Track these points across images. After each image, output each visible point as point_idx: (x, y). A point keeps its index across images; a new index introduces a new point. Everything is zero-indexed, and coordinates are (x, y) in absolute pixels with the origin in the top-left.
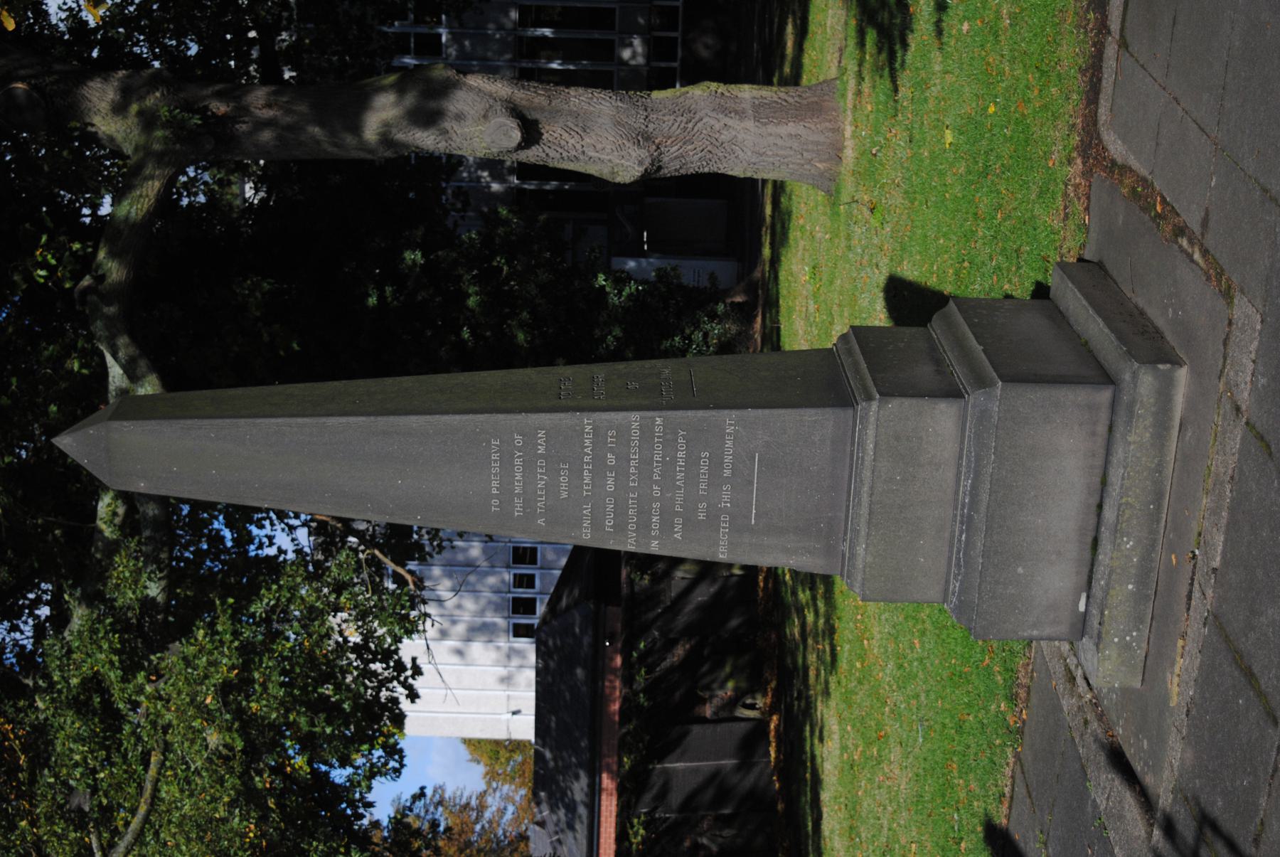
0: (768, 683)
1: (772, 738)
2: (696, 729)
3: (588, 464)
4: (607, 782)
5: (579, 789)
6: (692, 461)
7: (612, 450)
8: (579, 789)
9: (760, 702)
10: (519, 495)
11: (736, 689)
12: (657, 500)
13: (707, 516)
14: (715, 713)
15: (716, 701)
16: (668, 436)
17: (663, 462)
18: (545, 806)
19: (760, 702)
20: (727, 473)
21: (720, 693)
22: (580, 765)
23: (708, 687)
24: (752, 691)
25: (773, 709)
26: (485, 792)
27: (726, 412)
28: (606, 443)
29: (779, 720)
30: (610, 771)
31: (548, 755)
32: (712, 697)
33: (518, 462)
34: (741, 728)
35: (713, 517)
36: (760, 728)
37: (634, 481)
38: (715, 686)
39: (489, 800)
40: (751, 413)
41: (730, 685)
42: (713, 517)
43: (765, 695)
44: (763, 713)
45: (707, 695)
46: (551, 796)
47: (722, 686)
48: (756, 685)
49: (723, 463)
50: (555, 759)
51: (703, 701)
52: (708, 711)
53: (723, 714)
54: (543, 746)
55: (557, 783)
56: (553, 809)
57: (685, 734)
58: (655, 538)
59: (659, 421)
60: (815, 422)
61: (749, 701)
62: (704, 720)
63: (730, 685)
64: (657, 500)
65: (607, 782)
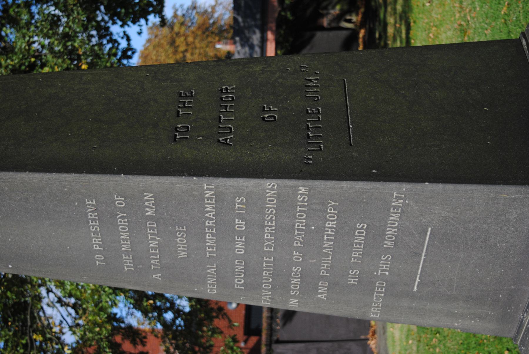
0: (359, 8)
1: (361, 41)
2: (319, 35)
3: (209, 228)
4: (270, 36)
5: (256, 38)
6: (344, 233)
7: (240, 216)
8: (256, 38)
9: (354, 18)
10: (127, 253)
11: (341, 10)
12: (297, 264)
13: (359, 282)
14: (329, 24)
15: (330, 17)
16: (314, 207)
17: (307, 230)
18: (238, 44)
19: (354, 18)
20: (388, 244)
21: (332, 12)
22: (257, 26)
23: (326, 8)
24: (349, 12)
25: (362, 24)
26: (215, 5)
27: (394, 185)
28: (234, 209)
29: (365, 32)
30: (272, 31)
31: (240, 19)
32: (328, 14)
33: (122, 222)
34: (345, 33)
35: (366, 285)
36: (354, 34)
37: (269, 246)
38: (330, 7)
39: (217, 9)
40: (428, 187)
41: (338, 7)
42: (366, 285)
43: (357, 15)
44: (356, 26)
45: (325, 12)
46: (241, 39)
47: (334, 8)
48: (352, 8)
49: (384, 235)
50: (244, 22)
51: (322, 16)
52: (325, 22)
53: (334, 25)
54: (238, 14)
55: (244, 34)
56: (243, 46)
57: (312, 37)
58: (294, 297)
59: (302, 190)
60: (514, 200)
61: (348, 17)
62: (322, 28)
63: (338, 7)
64: (297, 264)
65: (270, 36)
